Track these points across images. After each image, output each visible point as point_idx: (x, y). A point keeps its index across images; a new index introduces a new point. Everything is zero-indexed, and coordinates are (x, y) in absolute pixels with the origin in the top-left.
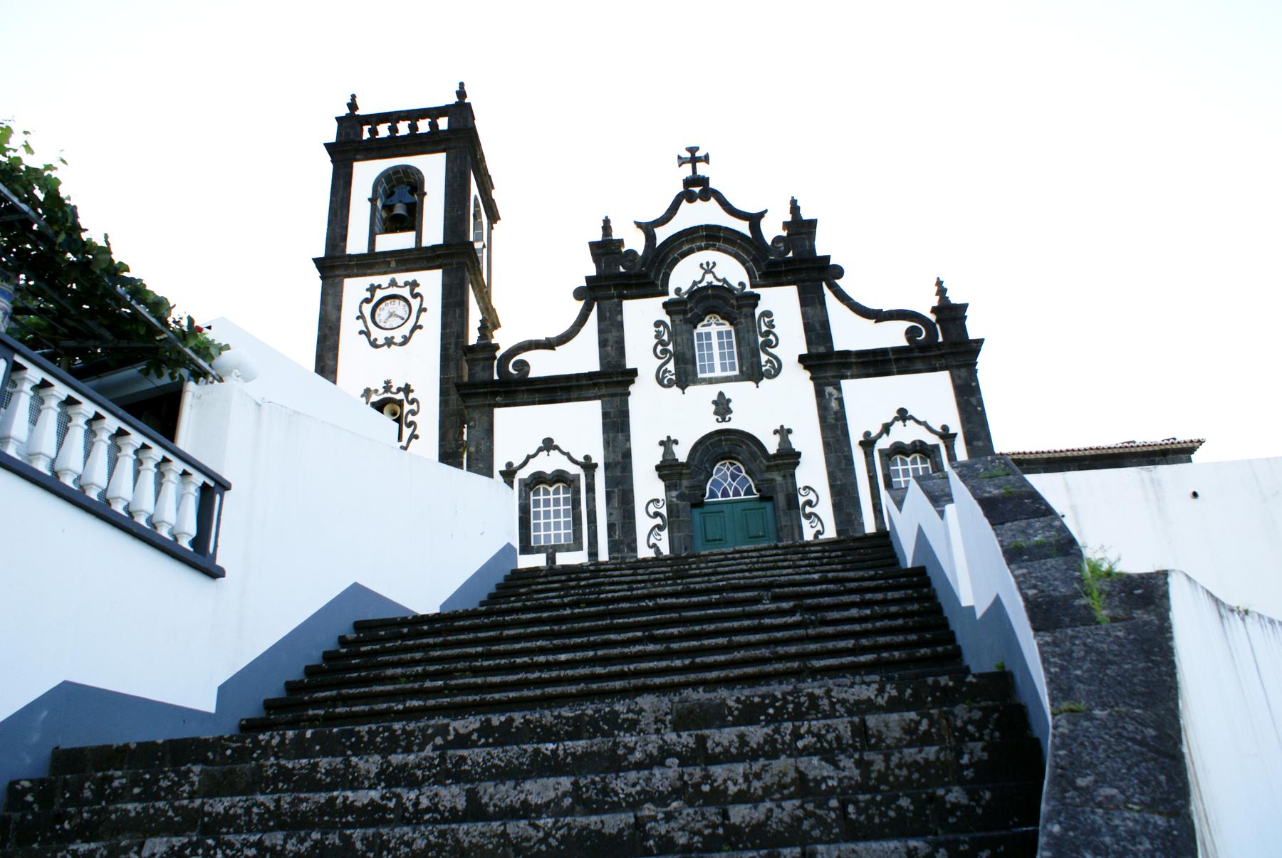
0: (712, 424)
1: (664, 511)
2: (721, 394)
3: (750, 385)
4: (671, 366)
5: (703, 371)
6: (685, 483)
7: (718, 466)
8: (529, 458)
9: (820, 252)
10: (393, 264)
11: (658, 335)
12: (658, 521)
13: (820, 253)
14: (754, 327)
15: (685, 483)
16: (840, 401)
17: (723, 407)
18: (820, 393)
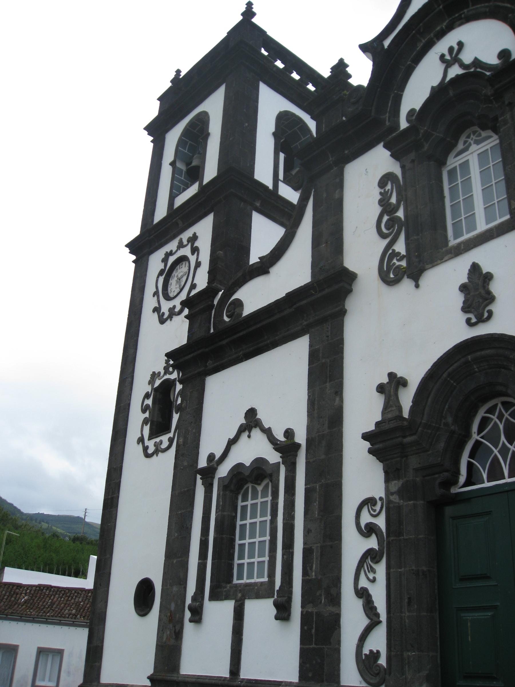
1: (381, 522)
2: (475, 268)
4: (400, 247)
5: (457, 235)
6: (414, 462)
7: (481, 414)
8: (232, 442)
10: (180, 223)
11: (384, 202)
12: (373, 543)
13: (330, 74)
15: (414, 462)
17: (478, 295)
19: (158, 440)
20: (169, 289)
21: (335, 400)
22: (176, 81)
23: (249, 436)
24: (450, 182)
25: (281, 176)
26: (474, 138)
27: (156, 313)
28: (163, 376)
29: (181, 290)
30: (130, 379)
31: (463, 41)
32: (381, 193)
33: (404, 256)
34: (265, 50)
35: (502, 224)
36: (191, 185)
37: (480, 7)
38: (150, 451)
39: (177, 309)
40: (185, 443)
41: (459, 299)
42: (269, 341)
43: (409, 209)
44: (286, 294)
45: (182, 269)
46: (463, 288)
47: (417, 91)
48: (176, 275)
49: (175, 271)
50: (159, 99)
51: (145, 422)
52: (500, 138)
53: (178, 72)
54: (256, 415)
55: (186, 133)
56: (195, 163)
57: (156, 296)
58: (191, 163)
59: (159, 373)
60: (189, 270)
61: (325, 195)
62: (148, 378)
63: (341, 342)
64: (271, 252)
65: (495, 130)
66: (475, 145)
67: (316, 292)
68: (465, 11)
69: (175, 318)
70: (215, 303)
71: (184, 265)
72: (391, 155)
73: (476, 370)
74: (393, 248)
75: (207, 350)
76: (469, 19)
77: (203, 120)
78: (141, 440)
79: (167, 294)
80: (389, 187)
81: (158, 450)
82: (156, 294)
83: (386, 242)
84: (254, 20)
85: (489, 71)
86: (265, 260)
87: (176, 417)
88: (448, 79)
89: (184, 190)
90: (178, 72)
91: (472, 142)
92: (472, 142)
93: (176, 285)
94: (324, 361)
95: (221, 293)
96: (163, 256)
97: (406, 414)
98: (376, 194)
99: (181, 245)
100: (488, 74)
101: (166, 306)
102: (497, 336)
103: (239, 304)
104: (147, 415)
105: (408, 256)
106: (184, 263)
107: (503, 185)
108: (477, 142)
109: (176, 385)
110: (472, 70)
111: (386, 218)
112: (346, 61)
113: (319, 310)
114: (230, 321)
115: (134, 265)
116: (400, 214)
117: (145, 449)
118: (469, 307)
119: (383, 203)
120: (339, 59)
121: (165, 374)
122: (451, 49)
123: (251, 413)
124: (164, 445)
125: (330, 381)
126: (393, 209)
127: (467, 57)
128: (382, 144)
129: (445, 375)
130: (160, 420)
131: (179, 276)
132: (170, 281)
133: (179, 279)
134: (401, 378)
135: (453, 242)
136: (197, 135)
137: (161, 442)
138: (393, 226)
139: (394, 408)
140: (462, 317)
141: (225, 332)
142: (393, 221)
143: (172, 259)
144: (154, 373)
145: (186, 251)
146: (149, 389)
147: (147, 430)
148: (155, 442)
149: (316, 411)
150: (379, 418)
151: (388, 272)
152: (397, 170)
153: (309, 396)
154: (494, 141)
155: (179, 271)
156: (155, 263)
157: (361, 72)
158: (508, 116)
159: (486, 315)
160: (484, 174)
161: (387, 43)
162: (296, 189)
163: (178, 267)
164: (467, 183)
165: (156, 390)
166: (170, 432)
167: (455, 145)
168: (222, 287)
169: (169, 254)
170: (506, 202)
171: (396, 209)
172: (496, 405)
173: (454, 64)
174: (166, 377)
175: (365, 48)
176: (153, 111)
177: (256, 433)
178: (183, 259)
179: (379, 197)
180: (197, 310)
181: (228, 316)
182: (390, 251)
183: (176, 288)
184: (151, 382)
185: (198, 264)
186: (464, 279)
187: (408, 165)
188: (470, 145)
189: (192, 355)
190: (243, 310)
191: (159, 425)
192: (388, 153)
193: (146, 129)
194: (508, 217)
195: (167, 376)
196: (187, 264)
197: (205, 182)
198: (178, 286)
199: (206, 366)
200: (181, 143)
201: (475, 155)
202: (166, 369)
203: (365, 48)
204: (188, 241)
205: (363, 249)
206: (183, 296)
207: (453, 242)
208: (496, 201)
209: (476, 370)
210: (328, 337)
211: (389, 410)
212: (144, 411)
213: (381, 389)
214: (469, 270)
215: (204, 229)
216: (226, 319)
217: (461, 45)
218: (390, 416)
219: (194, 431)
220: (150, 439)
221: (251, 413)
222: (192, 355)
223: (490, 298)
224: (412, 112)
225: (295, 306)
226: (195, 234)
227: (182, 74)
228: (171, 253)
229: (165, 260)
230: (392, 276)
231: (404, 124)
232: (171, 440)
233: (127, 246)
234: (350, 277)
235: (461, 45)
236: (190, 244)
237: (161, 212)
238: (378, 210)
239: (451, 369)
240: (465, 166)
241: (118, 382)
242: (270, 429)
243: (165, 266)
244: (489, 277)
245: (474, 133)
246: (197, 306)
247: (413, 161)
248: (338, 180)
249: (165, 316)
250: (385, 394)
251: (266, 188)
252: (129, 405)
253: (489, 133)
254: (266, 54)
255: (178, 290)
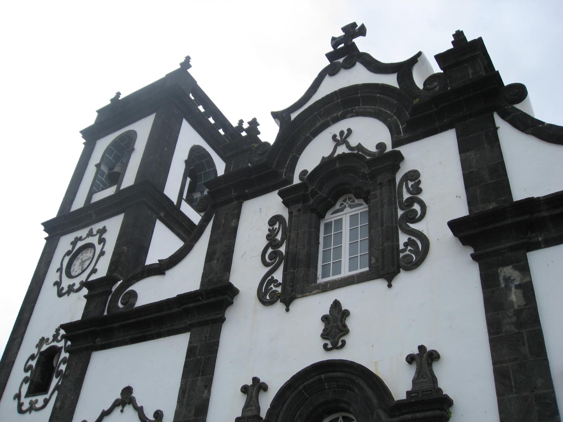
0: (314, 353)
2: (336, 304)
3: (379, 285)
4: (278, 275)
9: (451, 47)
11: (271, 237)
13: (451, 47)
14: (396, 194)
16: (528, 290)
17: (336, 326)
18: (489, 282)
19: (34, 399)
20: (72, 268)
21: (203, 392)
22: (115, 101)
23: (122, 411)
24: (325, 233)
25: (184, 197)
26: (349, 203)
27: (56, 286)
28: (51, 342)
29: (83, 271)
30: (20, 340)
31: (352, 129)
32: (269, 230)
33: (280, 284)
34: (193, 95)
35: (362, 273)
36: (109, 187)
37: (369, 108)
38: (24, 408)
39: (76, 287)
40: (61, 407)
41: (320, 327)
42: (154, 332)
43: (291, 247)
44: (178, 296)
45: (87, 254)
46: (325, 319)
47: (311, 158)
48: (81, 257)
49: (80, 255)
50: (98, 111)
51: (25, 380)
52: (369, 207)
53: (119, 94)
54: (132, 393)
55: (115, 144)
56: (117, 169)
57: (59, 272)
58: (113, 169)
59: (48, 339)
60: (94, 256)
61: (223, 221)
62: (37, 341)
63: (217, 344)
64: (170, 257)
65: (367, 201)
66: (349, 208)
67: (203, 299)
68: (357, 107)
69: (72, 295)
70: (114, 289)
71: (89, 251)
72: (283, 202)
73: (327, 387)
74: (273, 275)
75: (99, 328)
76: (358, 114)
77: (131, 137)
78: (18, 396)
79: (70, 272)
80: (277, 226)
81: (32, 408)
82: (60, 270)
83: (268, 269)
84: (189, 71)
85: (368, 156)
86: (163, 263)
87: (55, 381)
88: (336, 155)
89: (103, 189)
90: (119, 94)
91: (347, 206)
92: (347, 206)
93: (79, 266)
94: (199, 357)
95: (119, 283)
96: (73, 240)
97: (263, 414)
98: (265, 229)
99: (90, 234)
100: (368, 158)
101: (66, 283)
102: (347, 363)
103: (134, 295)
104: (29, 374)
105: (284, 285)
106: (90, 249)
107: (367, 243)
108: (351, 207)
109: (61, 352)
110: (356, 152)
111: (270, 250)
112: (258, 121)
113: (202, 314)
114: (123, 308)
115: (45, 241)
116: (283, 249)
117: (20, 405)
118: (327, 335)
119: (270, 238)
120: (253, 117)
121: (53, 341)
122: (342, 133)
123: (127, 391)
124: (38, 405)
125: (202, 375)
126: (278, 244)
127: (353, 141)
128: (277, 191)
129: (301, 387)
130: (40, 381)
131: (84, 259)
132: (75, 262)
133: (83, 262)
134: (263, 383)
135: (321, 280)
136: (124, 146)
137: (37, 401)
138: (275, 258)
139: (253, 408)
140: (321, 342)
141: (116, 316)
142: (276, 254)
143: (80, 244)
144: (43, 338)
145: (94, 240)
146: (35, 351)
147: (25, 387)
148: (31, 401)
149: (185, 399)
150: (240, 415)
151: (265, 294)
152: (285, 214)
153: (181, 385)
154: (364, 208)
155: (84, 255)
156: (65, 243)
157: (269, 133)
158: (378, 192)
159: (340, 343)
160: (353, 232)
161: (294, 116)
162: (198, 211)
163: (84, 251)
164: (339, 236)
165: (42, 354)
166: (47, 393)
167: (334, 205)
168: (121, 277)
169: (78, 239)
170: (367, 256)
171: (280, 245)
172: (338, 418)
173: (343, 144)
174: (53, 344)
175: (275, 115)
176: (90, 120)
177: (129, 409)
178: (90, 246)
179: (268, 233)
180: (96, 292)
181: (122, 303)
182: (270, 278)
183: (79, 269)
184: (39, 346)
185: (102, 253)
186: (327, 312)
187: (295, 213)
188: (345, 207)
189: (84, 331)
190: (136, 301)
191: (38, 385)
192: (280, 200)
193: (82, 132)
194: (367, 269)
195: (55, 344)
196: (93, 251)
197: (123, 187)
198: (80, 267)
199: (95, 342)
200: (108, 150)
201: (348, 216)
202: (55, 338)
203: (275, 115)
204: (98, 232)
205: (247, 271)
206: (83, 277)
207: (321, 280)
208: (359, 255)
209: (327, 387)
210: (206, 337)
211: (249, 409)
212: (26, 370)
213: (245, 389)
214: (331, 305)
215: (114, 226)
216: (120, 305)
217: (350, 131)
218: (249, 414)
219: (72, 398)
220: (27, 396)
221: (127, 391)
222: (84, 331)
223: (345, 331)
224: (304, 172)
225: (183, 307)
226: (104, 228)
227: (121, 97)
228: (80, 239)
229: (74, 244)
230: (268, 298)
231: (296, 180)
232: (46, 402)
233: (43, 224)
234: (232, 292)
235: (350, 131)
236: (98, 235)
237: (79, 203)
238: (265, 242)
239: (306, 383)
240: (339, 222)
241: (8, 340)
242: (142, 407)
243: (73, 248)
244: (346, 313)
245: (350, 199)
246: (97, 290)
247: (299, 210)
248: (236, 212)
249: (64, 291)
250: (248, 395)
251: (171, 202)
252: (14, 362)
253: (361, 201)
254: (193, 98)
255: (80, 271)
